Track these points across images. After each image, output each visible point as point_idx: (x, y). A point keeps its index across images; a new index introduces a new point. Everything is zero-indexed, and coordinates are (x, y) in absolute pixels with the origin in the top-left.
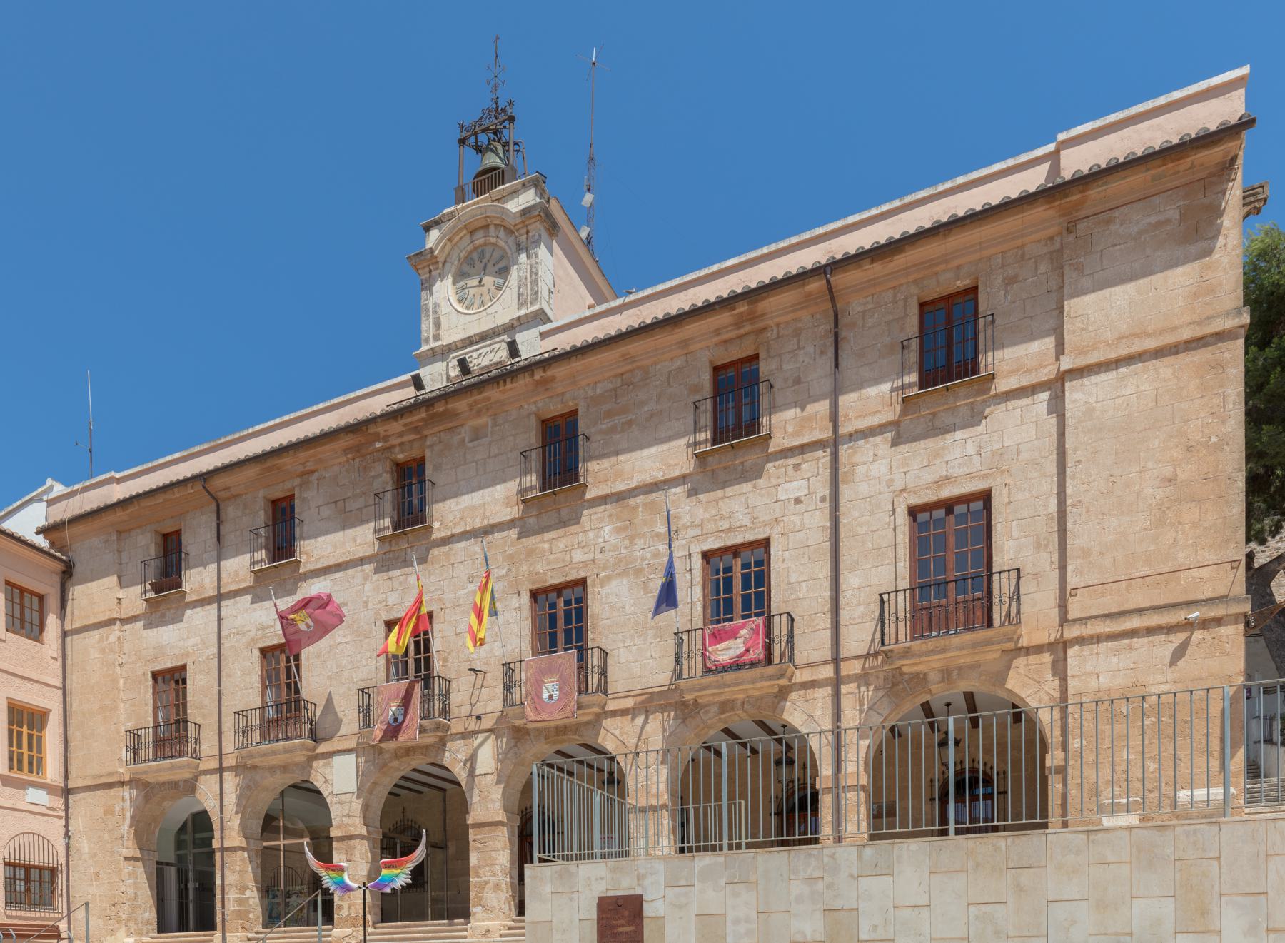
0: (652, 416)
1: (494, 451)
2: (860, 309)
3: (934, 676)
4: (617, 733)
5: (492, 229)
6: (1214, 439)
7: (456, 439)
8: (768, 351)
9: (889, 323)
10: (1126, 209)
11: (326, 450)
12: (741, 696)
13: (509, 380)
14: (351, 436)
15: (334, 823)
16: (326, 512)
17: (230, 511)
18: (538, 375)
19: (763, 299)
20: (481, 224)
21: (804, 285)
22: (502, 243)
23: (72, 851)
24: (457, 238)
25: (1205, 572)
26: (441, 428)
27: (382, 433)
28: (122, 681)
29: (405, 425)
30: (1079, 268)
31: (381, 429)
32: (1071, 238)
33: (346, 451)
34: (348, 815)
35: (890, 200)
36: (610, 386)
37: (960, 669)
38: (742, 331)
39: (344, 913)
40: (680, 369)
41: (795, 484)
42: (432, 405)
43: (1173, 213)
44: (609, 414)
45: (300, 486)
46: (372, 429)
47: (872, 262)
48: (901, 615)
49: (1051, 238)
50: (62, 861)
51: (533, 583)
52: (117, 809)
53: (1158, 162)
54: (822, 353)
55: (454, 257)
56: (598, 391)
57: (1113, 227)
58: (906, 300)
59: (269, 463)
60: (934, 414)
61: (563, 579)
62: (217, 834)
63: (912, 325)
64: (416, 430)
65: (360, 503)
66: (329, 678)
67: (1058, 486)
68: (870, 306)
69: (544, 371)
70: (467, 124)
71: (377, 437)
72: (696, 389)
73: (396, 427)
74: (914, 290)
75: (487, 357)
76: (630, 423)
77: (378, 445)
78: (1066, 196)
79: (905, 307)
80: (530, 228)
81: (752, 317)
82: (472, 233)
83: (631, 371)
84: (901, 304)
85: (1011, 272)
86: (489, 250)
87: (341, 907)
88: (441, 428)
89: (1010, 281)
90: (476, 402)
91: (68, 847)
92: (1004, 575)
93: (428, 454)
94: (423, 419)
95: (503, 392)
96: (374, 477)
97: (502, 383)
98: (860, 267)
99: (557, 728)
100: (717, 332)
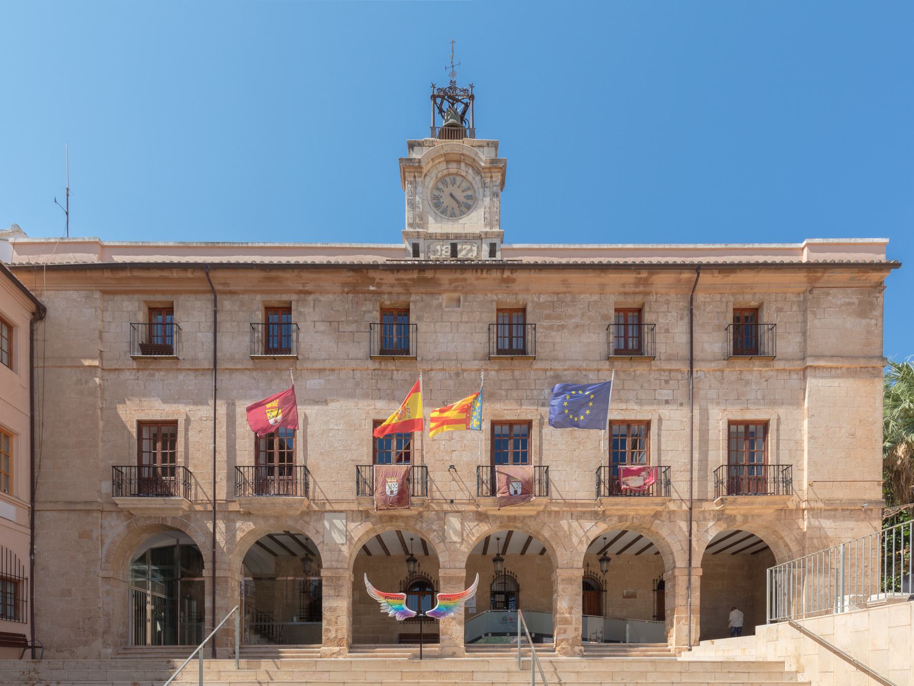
0: (577, 326)
1: (465, 319)
2: (703, 300)
3: (739, 518)
4: (552, 525)
5: (463, 165)
6: (870, 419)
7: (435, 302)
8: (650, 308)
9: (718, 313)
10: (835, 290)
11: (326, 280)
12: (632, 513)
13: (485, 271)
14: (351, 274)
15: (324, 565)
16: (321, 327)
17: (227, 304)
18: (507, 274)
19: (657, 273)
20: (456, 157)
21: (681, 273)
22: (470, 178)
23: (37, 568)
24: (437, 162)
25: (867, 485)
26: (424, 290)
27: (377, 280)
28: (101, 423)
29: (397, 280)
30: (815, 314)
31: (376, 275)
32: (811, 297)
33: (344, 284)
34: (337, 561)
35: (721, 242)
36: (550, 299)
37: (753, 516)
38: (637, 290)
39: (332, 635)
40: (596, 302)
41: (665, 391)
42: (424, 271)
43: (855, 300)
44: (548, 317)
45: (298, 301)
46: (371, 274)
47: (719, 273)
48: (133, 477)
49: (799, 294)
50: (27, 574)
51: (494, 416)
52: (95, 534)
53: (856, 270)
54: (681, 318)
55: (433, 174)
56: (541, 300)
57: (830, 298)
58: (727, 302)
59: (274, 274)
60: (741, 371)
61: (516, 418)
62: (208, 565)
63: (730, 318)
64: (405, 286)
65: (353, 327)
66: (321, 454)
67: (707, 425)
68: (708, 300)
69: (512, 273)
70: (437, 87)
71: (372, 281)
72: (605, 317)
73: (389, 278)
74: (731, 299)
75: (442, 252)
76: (563, 327)
77: (372, 288)
78: (816, 272)
79: (727, 307)
80: (493, 174)
81: (646, 282)
82: (448, 162)
83: (564, 293)
84: (724, 304)
85: (780, 306)
86: (459, 179)
87: (328, 630)
88: (424, 290)
89: (780, 310)
90: (456, 280)
91: (32, 563)
92: (772, 468)
93: (412, 307)
94: (412, 280)
95: (477, 279)
96: (365, 312)
97: (479, 271)
98: (712, 273)
99: (509, 516)
100: (624, 285)
